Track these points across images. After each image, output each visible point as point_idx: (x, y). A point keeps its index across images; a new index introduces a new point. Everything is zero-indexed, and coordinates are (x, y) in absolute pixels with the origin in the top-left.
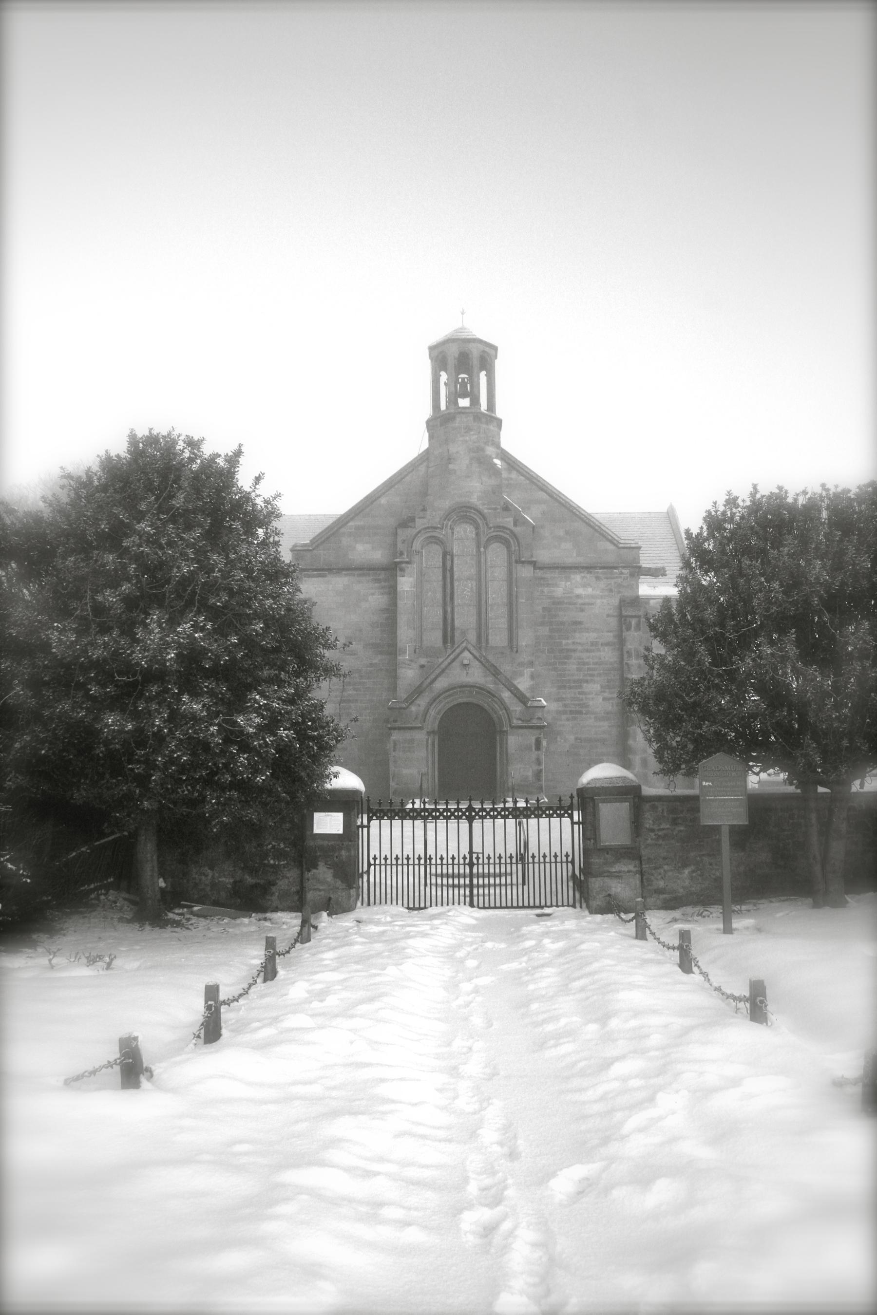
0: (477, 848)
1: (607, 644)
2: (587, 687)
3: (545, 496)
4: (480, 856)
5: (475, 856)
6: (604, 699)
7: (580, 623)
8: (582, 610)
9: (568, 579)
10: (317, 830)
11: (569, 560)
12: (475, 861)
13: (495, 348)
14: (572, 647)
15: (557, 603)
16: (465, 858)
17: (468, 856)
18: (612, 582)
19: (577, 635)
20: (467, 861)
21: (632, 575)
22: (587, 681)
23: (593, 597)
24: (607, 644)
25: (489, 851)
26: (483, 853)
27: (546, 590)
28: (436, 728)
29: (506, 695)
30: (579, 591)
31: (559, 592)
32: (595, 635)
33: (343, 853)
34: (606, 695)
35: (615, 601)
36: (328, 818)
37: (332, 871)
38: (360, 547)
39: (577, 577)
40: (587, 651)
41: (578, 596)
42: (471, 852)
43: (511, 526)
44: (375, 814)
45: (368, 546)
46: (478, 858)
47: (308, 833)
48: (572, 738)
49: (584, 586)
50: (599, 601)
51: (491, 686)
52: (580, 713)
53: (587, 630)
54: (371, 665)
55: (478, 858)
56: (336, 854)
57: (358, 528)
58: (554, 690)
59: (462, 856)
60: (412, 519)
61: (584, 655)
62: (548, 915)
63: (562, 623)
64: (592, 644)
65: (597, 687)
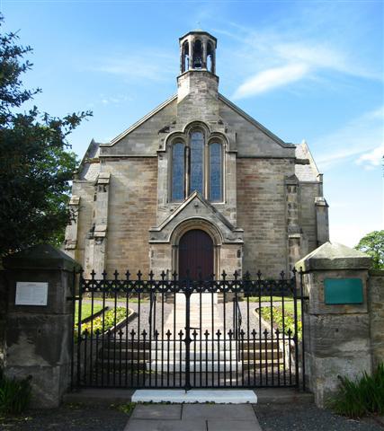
0: (194, 324)
1: (277, 200)
2: (266, 225)
3: (243, 119)
4: (198, 331)
5: (192, 331)
6: (276, 231)
7: (262, 188)
8: (263, 181)
9: (255, 164)
10: (20, 300)
11: (256, 154)
12: (192, 337)
13: (216, 40)
14: (257, 202)
15: (249, 177)
16: (181, 334)
17: (184, 331)
18: (280, 166)
19: (260, 195)
20: (184, 337)
21: (291, 162)
22: (265, 221)
23: (268, 174)
24: (277, 200)
25: (207, 326)
26: (200, 329)
27: (242, 169)
28: (178, 244)
29: (220, 224)
30: (261, 171)
31: (250, 171)
32: (269, 195)
33: (47, 326)
34: (277, 229)
35: (282, 177)
36: (32, 289)
37: (34, 346)
38: (138, 145)
39: (260, 163)
40: (266, 204)
41: (261, 174)
42: (188, 328)
43: (224, 133)
44: (289, 286)
45: (143, 145)
46: (195, 334)
47: (10, 304)
48: (257, 253)
49: (264, 168)
50: (272, 177)
51: (209, 219)
52: (262, 239)
53: (266, 192)
54: (143, 210)
55: (195, 334)
56: (39, 328)
57: (137, 134)
58: (247, 226)
59: (178, 331)
60: (168, 128)
61: (264, 206)
62: (148, 134)
63: (252, 188)
64: (269, 200)
65: (271, 224)
